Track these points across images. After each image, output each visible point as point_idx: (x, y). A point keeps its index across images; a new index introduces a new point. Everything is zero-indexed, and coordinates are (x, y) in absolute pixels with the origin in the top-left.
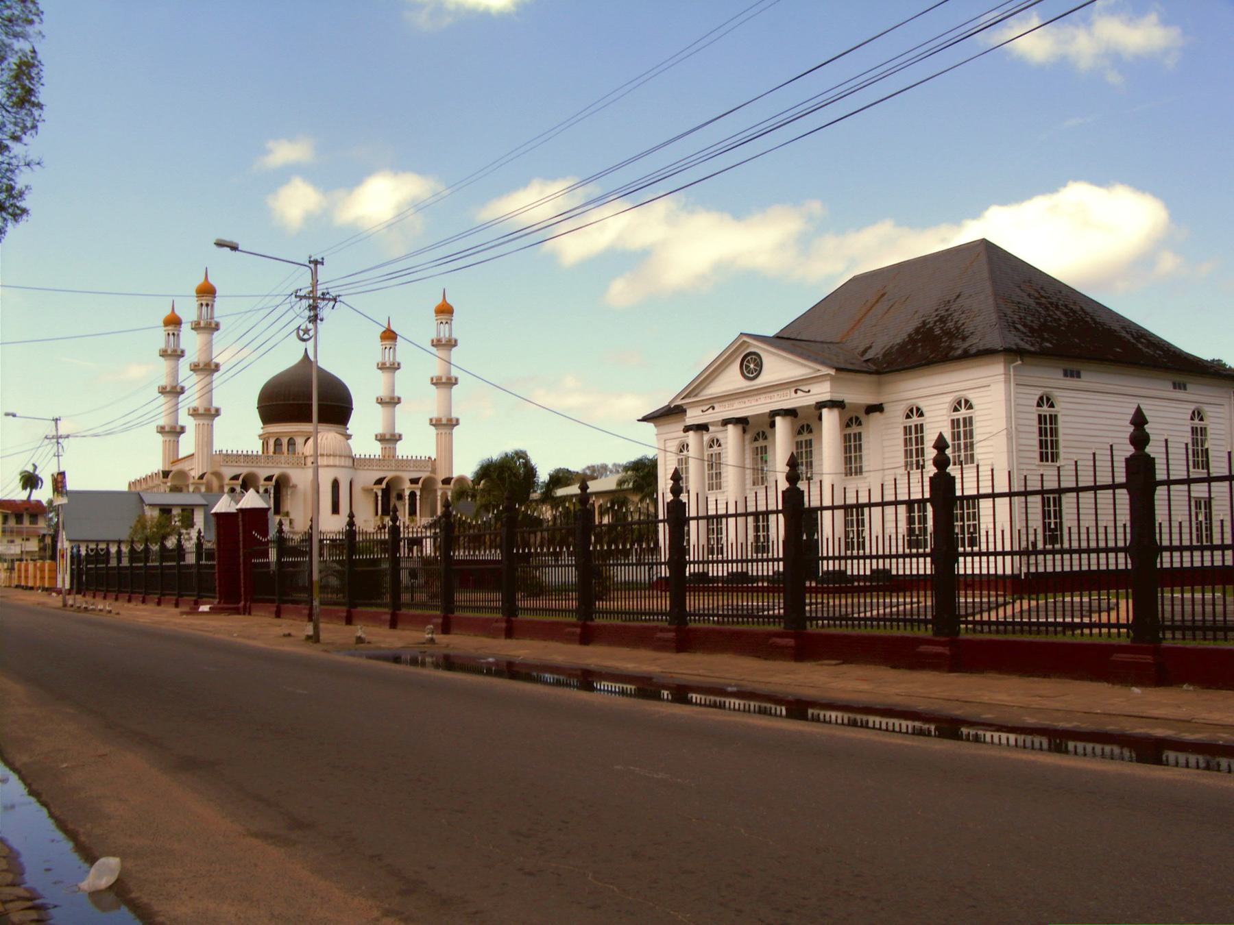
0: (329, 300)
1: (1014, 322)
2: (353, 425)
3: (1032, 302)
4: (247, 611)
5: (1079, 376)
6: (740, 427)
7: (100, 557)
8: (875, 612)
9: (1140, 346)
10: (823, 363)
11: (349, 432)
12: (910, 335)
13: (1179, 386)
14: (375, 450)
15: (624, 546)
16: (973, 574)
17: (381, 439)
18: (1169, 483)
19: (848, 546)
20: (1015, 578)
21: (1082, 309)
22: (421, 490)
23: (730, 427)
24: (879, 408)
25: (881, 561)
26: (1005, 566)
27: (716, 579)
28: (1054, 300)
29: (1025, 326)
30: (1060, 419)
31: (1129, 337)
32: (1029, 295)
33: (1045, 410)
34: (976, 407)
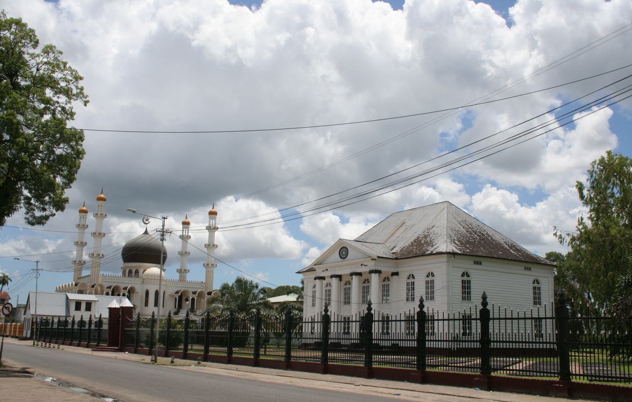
1: (454, 240)
3: (464, 230)
5: (481, 264)
6: (338, 279)
9: (511, 251)
16: (494, 348)
18: (494, 319)
21: (487, 234)
22: (197, 297)
23: (334, 278)
24: (396, 274)
26: (445, 345)
28: (475, 229)
29: (459, 241)
31: (507, 247)
32: (464, 227)
33: (465, 278)
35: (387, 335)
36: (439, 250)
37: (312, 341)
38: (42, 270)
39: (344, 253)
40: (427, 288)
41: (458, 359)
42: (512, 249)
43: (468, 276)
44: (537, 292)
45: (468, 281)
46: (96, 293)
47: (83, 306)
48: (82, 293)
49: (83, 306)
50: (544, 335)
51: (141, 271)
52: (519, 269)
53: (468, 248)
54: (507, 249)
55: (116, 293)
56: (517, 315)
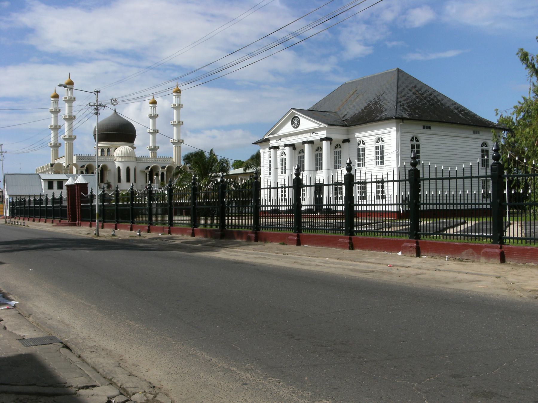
1: (403, 105)
2: (136, 142)
4: (79, 225)
5: (430, 128)
6: (292, 148)
7: (22, 202)
8: (373, 229)
9: (460, 115)
10: (323, 122)
11: (134, 146)
12: (362, 110)
13: (476, 132)
15: (248, 199)
16: (388, 211)
19: (378, 197)
20: (398, 212)
21: (437, 99)
23: (287, 148)
24: (347, 141)
27: (282, 212)
31: (456, 111)
32: (413, 93)
33: (414, 143)
34: (385, 141)
35: (382, 199)
37: (269, 209)
38: (6, 152)
39: (296, 122)
40: (377, 153)
42: (462, 114)
43: (418, 141)
47: (55, 185)
48: (59, 173)
49: (55, 185)
50: (387, 196)
52: (468, 133)
53: (418, 114)
54: (456, 113)
55: (90, 171)
56: (448, 174)
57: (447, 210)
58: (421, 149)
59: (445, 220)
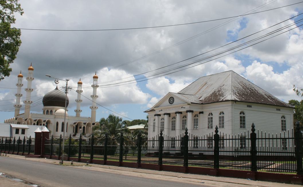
0: (70, 89)
5: (251, 107)
6: (168, 115)
9: (269, 99)
12: (211, 94)
14: (74, 114)
17: (76, 111)
18: (258, 139)
22: (86, 126)
23: (166, 115)
24: (202, 113)
25: (191, 152)
26: (230, 154)
27: (173, 154)
28: (248, 87)
30: (246, 117)
31: (266, 97)
32: (241, 86)
33: (242, 115)
36: (226, 99)
37: (153, 152)
40: (220, 121)
41: (238, 162)
42: (269, 98)
43: (244, 114)
44: (284, 123)
45: (243, 117)
46: (28, 124)
47: (20, 131)
49: (20, 131)
50: (288, 148)
51: (54, 111)
52: (273, 110)
53: (244, 98)
55: (39, 124)
56: (272, 136)
57: (260, 156)
58: (286, 122)
59: (206, 161)
